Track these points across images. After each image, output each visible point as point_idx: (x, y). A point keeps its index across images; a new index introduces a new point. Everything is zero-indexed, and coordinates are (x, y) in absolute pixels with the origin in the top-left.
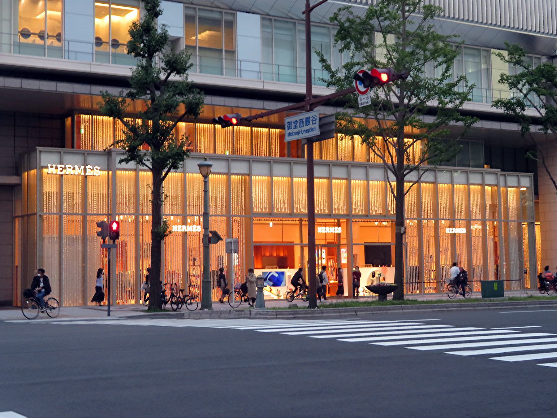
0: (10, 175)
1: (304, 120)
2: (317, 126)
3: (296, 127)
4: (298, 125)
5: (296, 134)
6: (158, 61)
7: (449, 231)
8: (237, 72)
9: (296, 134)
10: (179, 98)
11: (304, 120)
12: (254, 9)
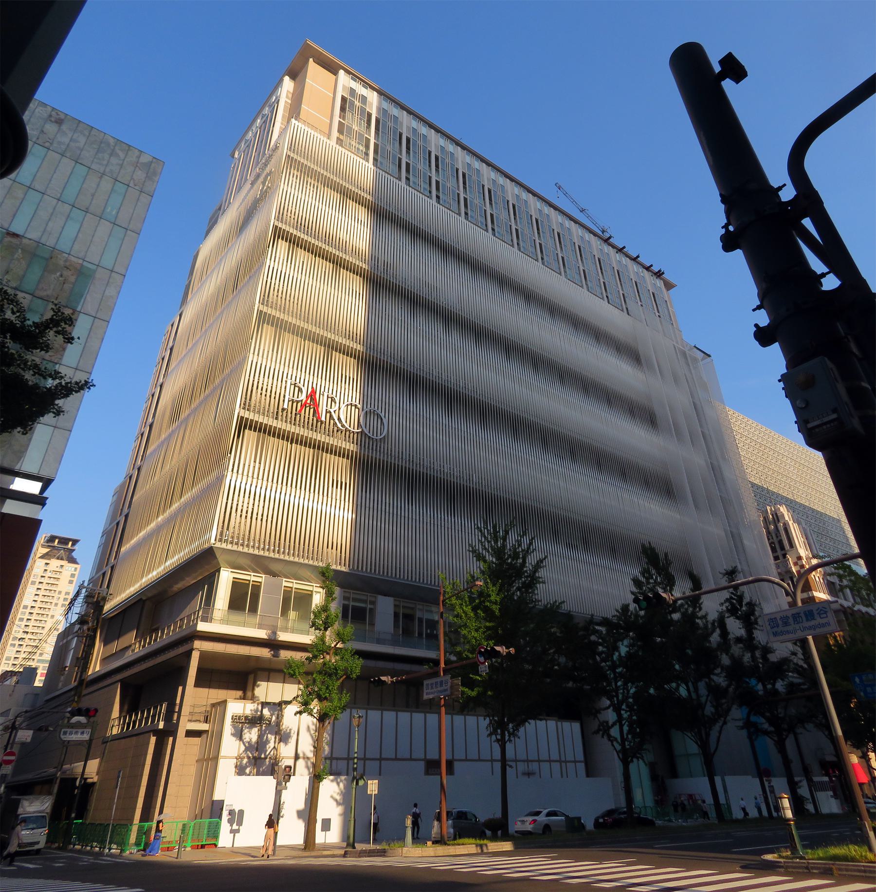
1: (802, 615)
4: (791, 620)
5: (788, 632)
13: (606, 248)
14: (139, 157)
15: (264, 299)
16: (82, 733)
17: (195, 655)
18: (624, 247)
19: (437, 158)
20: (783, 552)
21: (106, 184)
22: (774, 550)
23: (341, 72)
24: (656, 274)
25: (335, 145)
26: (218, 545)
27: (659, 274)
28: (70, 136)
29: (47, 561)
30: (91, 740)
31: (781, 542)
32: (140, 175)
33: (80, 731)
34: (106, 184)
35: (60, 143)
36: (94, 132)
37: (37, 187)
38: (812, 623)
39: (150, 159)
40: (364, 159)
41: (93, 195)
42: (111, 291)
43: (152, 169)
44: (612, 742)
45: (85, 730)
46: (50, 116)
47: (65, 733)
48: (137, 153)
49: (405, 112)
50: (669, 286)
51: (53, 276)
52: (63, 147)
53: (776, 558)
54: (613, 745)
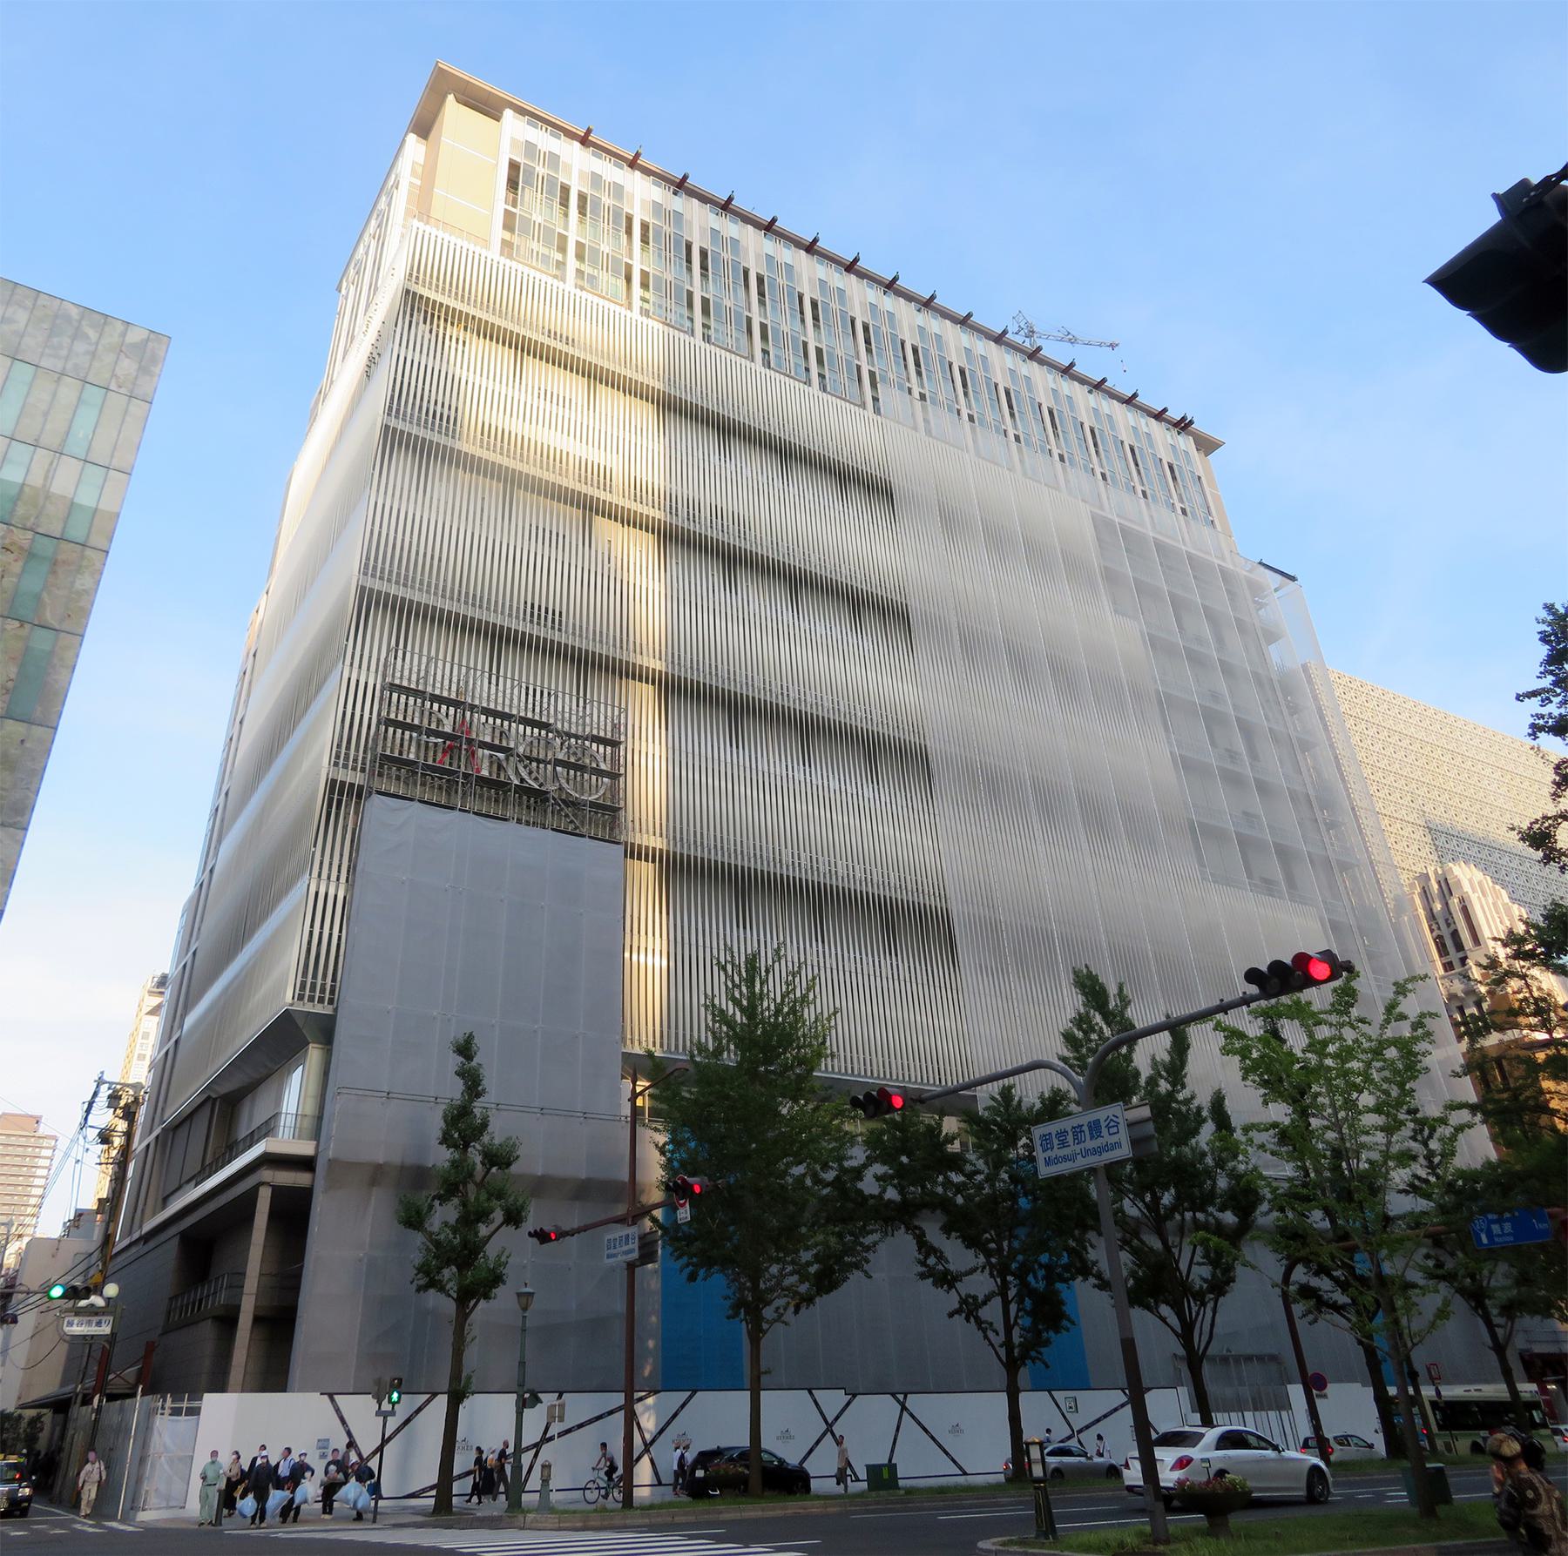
1: (1085, 1128)
2: (636, 1246)
3: (1063, 1144)
4: (1070, 1138)
5: (1065, 1159)
6: (475, 1156)
9: (1065, 1159)
10: (495, 1203)
11: (1085, 1128)
13: (1067, 387)
14: (124, 335)
15: (367, 565)
16: (99, 1324)
17: (265, 1196)
18: (1104, 380)
19: (814, 304)
20: (1461, 954)
21: (68, 391)
22: (1442, 950)
23: (508, 114)
24: (1176, 425)
25: (497, 257)
26: (299, 1007)
27: (1183, 425)
31: (1455, 935)
32: (127, 366)
34: (68, 391)
36: (42, 300)
38: (1066, 1151)
39: (145, 334)
40: (555, 277)
41: (46, 414)
42: (84, 581)
43: (148, 353)
44: (984, 1331)
45: (104, 1319)
47: (70, 1324)
48: (120, 327)
49: (695, 201)
50: (1207, 445)
53: (1448, 966)
54: (986, 1337)
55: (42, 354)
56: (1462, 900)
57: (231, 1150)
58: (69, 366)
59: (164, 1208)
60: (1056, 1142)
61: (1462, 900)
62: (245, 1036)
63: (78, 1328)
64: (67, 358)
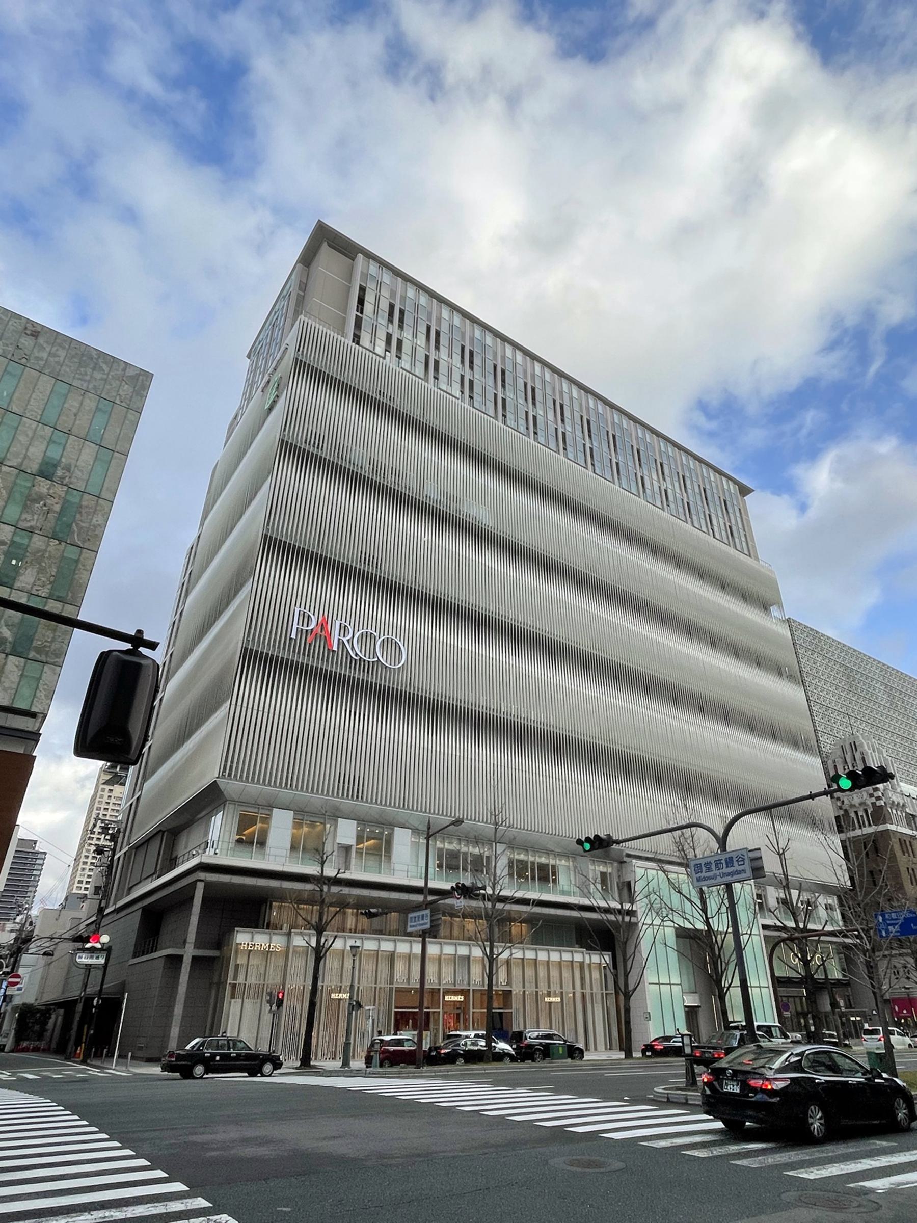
0: (211, 949)
1: (723, 862)
2: (429, 921)
7: (547, 1000)
8: (392, 871)
12: (407, 825)
14: (124, 370)
16: (98, 958)
17: (200, 887)
28: (48, 349)
29: (111, 788)
30: (105, 966)
33: (95, 955)
35: (38, 359)
37: (15, 409)
38: (730, 870)
42: (97, 519)
46: (26, 328)
51: (37, 505)
52: (42, 363)
55: (74, 378)
56: (862, 753)
57: (172, 863)
58: (91, 386)
59: (128, 894)
60: (704, 869)
61: (862, 753)
62: (199, 785)
63: (84, 959)
64: (89, 381)
